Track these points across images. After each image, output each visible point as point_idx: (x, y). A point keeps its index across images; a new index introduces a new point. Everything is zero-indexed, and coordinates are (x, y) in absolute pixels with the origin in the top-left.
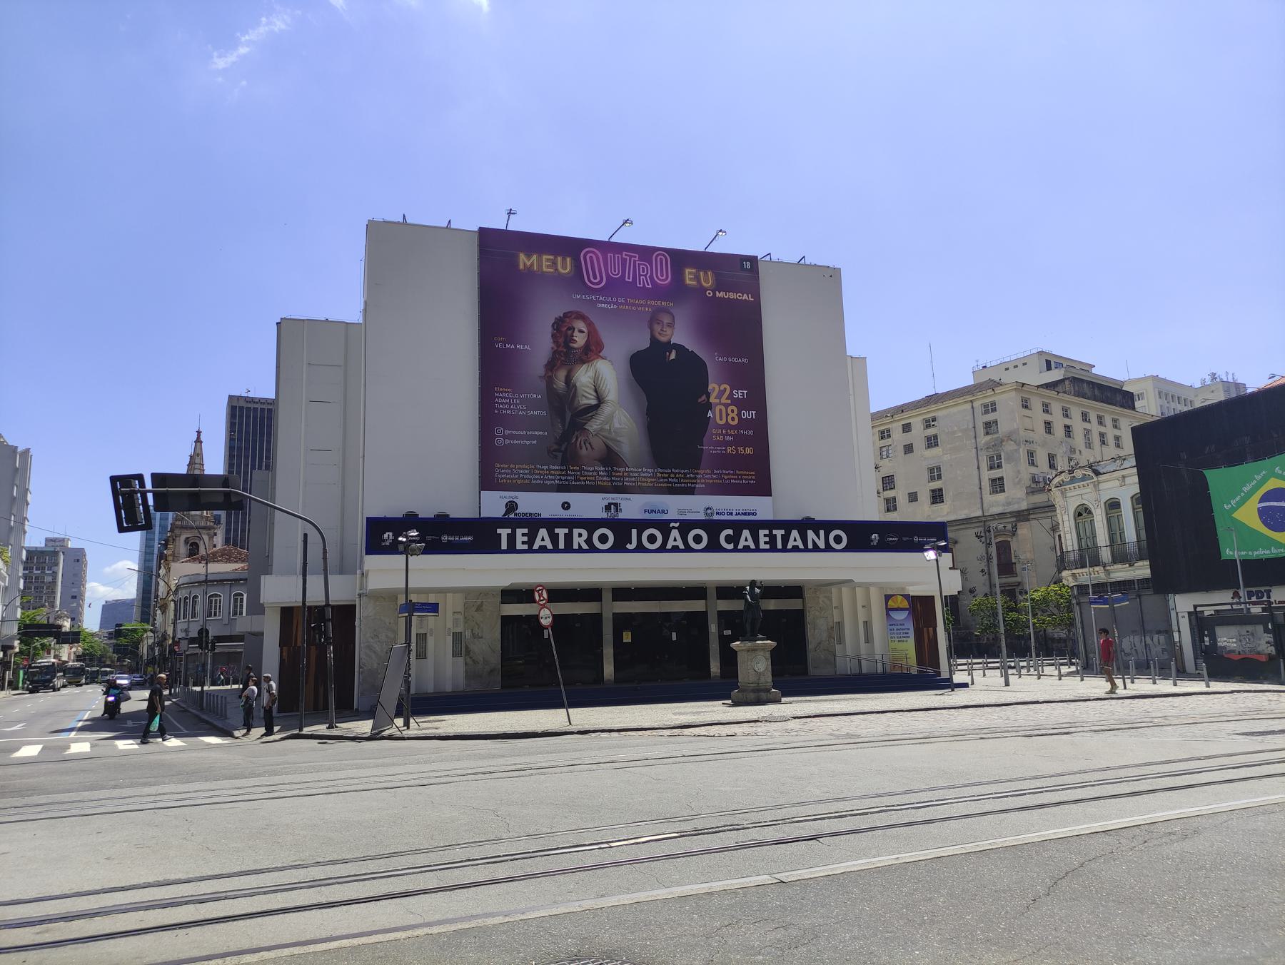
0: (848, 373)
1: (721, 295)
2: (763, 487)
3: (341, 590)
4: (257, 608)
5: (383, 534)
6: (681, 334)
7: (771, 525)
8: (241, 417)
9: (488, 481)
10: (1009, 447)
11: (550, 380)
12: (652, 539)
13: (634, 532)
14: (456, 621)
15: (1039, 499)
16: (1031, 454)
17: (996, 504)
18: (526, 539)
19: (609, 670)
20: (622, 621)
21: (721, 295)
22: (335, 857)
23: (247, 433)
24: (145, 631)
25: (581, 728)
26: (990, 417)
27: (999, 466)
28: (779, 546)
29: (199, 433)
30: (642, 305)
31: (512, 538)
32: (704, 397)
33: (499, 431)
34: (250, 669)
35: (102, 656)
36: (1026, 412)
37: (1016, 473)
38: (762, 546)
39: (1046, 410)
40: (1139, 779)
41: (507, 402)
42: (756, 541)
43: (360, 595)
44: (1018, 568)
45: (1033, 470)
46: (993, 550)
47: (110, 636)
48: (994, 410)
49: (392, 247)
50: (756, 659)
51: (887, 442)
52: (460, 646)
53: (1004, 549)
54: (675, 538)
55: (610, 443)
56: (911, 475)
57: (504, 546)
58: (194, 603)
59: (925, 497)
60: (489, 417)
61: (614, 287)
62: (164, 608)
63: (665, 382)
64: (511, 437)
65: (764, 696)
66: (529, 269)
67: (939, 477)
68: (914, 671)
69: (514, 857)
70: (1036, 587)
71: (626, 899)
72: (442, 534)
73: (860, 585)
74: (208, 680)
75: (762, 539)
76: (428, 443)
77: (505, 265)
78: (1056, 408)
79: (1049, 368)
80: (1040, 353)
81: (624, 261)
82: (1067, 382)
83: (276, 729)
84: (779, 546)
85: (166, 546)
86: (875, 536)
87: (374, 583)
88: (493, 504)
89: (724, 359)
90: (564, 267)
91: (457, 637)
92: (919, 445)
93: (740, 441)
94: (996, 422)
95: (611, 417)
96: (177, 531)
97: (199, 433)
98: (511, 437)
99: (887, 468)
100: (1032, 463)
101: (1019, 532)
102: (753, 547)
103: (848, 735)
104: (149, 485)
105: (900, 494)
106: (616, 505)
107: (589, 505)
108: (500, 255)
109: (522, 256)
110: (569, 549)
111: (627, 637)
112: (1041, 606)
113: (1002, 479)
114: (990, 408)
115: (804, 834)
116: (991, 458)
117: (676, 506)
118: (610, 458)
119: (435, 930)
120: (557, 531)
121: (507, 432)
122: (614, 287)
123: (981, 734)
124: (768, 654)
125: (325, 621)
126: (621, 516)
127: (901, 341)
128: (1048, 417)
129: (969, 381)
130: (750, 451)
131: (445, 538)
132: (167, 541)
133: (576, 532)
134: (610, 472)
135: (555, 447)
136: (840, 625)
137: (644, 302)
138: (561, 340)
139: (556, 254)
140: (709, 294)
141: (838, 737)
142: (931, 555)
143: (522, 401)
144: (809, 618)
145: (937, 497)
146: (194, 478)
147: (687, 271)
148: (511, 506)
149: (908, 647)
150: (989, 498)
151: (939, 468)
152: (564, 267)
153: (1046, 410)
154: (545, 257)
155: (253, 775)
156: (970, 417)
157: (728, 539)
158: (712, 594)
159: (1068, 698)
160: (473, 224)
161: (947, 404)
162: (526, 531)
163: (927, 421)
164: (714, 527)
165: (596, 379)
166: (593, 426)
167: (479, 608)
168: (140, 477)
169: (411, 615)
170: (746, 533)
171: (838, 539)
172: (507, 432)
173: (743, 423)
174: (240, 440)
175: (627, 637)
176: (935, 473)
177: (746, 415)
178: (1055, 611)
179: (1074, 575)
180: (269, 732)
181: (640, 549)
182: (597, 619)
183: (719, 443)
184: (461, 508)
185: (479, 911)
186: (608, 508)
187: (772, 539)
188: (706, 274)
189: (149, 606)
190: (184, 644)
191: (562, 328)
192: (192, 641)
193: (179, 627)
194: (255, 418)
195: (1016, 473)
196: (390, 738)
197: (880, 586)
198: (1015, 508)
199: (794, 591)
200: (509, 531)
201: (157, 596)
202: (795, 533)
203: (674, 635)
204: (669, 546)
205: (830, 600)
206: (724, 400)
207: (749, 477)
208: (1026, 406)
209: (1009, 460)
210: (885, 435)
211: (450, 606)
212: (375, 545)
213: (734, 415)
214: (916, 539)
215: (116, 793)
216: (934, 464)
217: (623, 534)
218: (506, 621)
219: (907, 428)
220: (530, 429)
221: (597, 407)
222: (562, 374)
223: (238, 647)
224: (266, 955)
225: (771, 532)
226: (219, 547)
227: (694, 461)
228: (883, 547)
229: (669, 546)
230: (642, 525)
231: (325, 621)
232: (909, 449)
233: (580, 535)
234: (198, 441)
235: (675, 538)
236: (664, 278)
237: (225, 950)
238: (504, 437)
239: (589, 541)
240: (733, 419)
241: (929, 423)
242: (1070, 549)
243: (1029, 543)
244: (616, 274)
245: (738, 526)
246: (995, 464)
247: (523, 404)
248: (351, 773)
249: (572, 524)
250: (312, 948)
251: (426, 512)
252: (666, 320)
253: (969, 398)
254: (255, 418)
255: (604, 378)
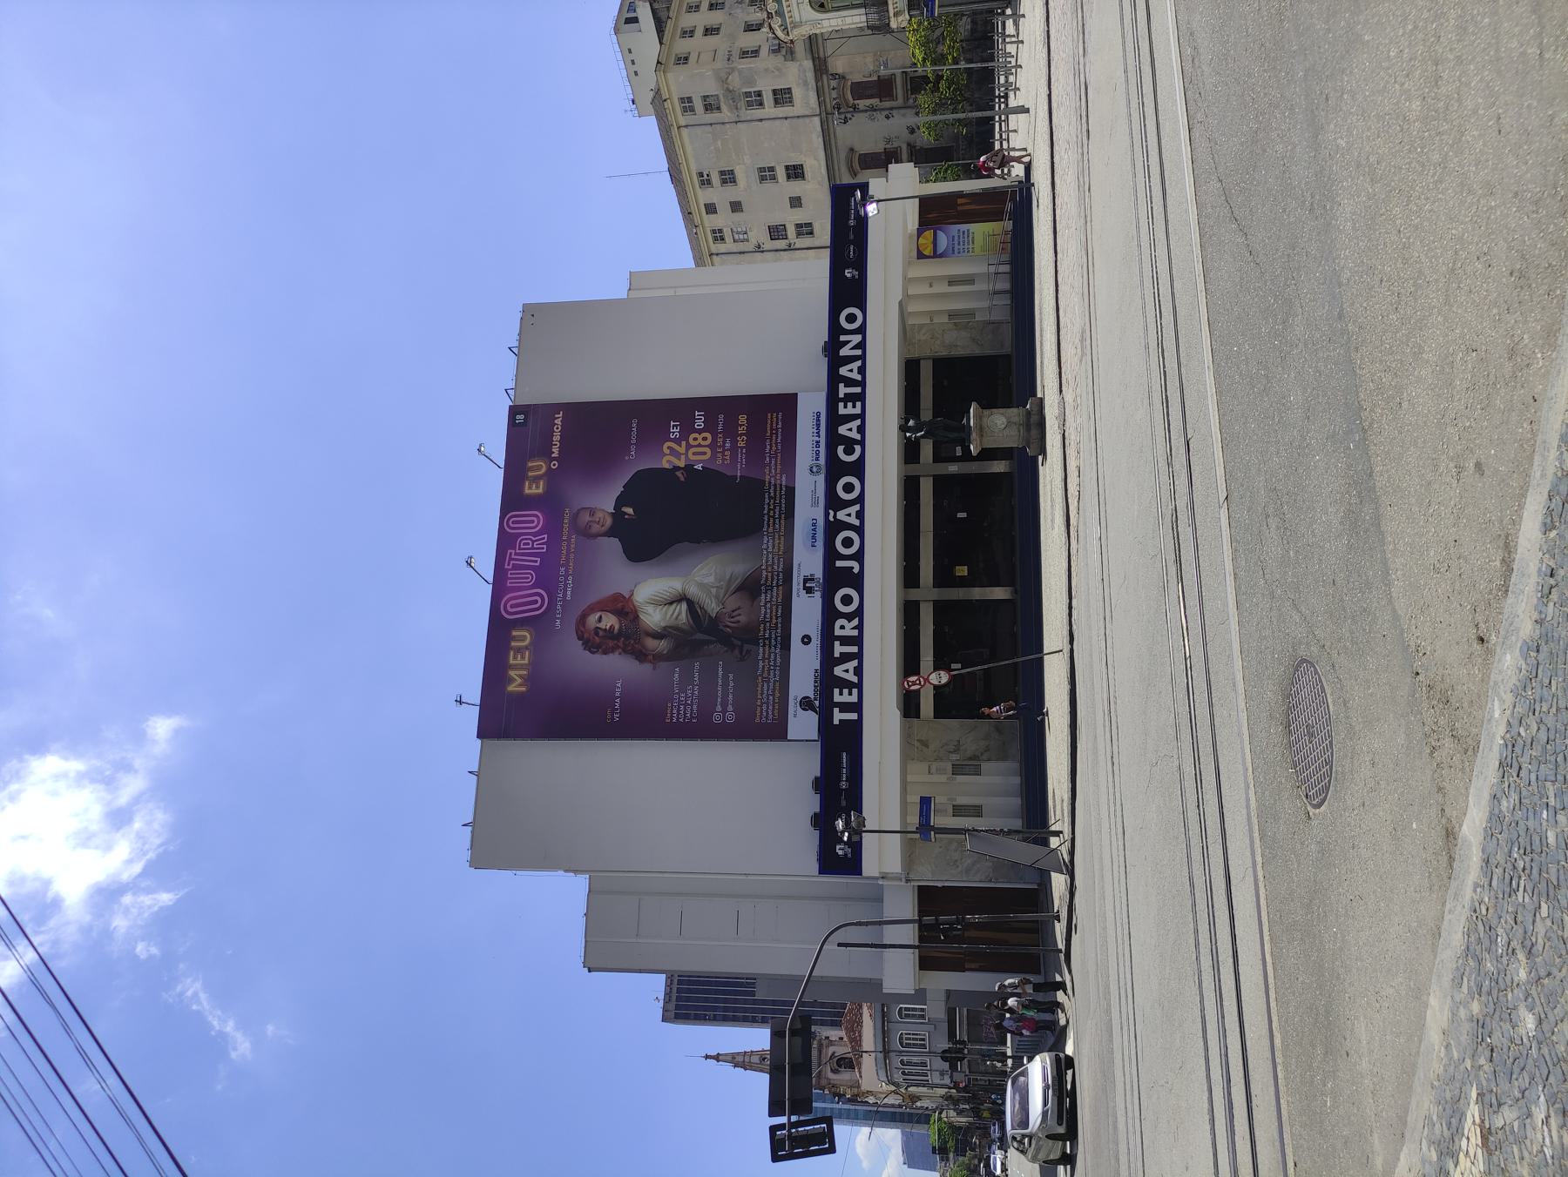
0: (645, 302)
1: (556, 450)
2: (786, 404)
3: (902, 904)
4: (920, 996)
5: (839, 857)
6: (604, 500)
7: (832, 400)
8: (687, 1007)
9: (776, 731)
10: (735, 81)
11: (658, 657)
12: (848, 543)
13: (839, 564)
14: (940, 771)
15: (800, 49)
16: (744, 54)
17: (805, 99)
18: (846, 691)
19: (1000, 593)
20: (943, 577)
21: (556, 450)
22: (1192, 941)
23: (706, 1000)
24: (940, 1119)
25: (1067, 640)
26: (698, 105)
27: (759, 94)
28: (858, 390)
29: (707, 1057)
30: (569, 546)
31: (845, 707)
32: (679, 474)
33: (717, 718)
34: (990, 1005)
35: (968, 1169)
36: (693, 59)
37: (768, 74)
38: (858, 410)
39: (689, 33)
40: (1137, 48)
41: (684, 706)
42: (852, 418)
43: (908, 881)
44: (883, 72)
45: (764, 52)
46: (862, 103)
47: (945, 1159)
48: (690, 100)
49: (499, 841)
50: (994, 426)
51: (727, 234)
52: (966, 766)
53: (860, 90)
54: (847, 515)
55: (733, 587)
56: (768, 205)
57: (854, 716)
58: (909, 1064)
59: (796, 188)
60: (700, 729)
61: (547, 578)
62: (915, 1098)
63: (664, 518)
64: (724, 705)
65: (1034, 419)
66: (527, 680)
67: (772, 169)
68: (1009, 225)
69: (1197, 760)
70: (906, 54)
71: (1238, 664)
72: (838, 791)
73: (905, 290)
74: (1000, 1048)
75: (850, 410)
76: (727, 805)
77: (520, 709)
78: (688, 20)
79: (635, 20)
80: (617, 30)
81: (515, 567)
82: (656, 6)
83: (1058, 978)
84: (858, 390)
85: (841, 1096)
86: (848, 273)
87: (894, 865)
88: (803, 724)
89: (633, 448)
90: (523, 639)
91: (958, 770)
92: (731, 193)
93: (731, 432)
94: (705, 98)
95: (701, 586)
96: (824, 1082)
97: (707, 1057)
98: (724, 705)
99: (759, 235)
100: (755, 53)
101: (840, 71)
102: (858, 422)
103: (1082, 340)
104: (783, 1120)
105: (791, 218)
106: (805, 581)
107: (806, 613)
108: (504, 716)
109: (511, 688)
110: (858, 641)
111: (962, 571)
112: (930, 47)
113: (775, 92)
114: (687, 104)
115: (1183, 450)
116: (749, 104)
117: (808, 509)
118: (750, 587)
119: (1259, 859)
120: (837, 655)
121: (719, 708)
122: (547, 578)
123: (1084, 188)
124: (987, 412)
125: (938, 923)
126: (819, 574)
127: (607, 223)
128: (699, 32)
129: (652, 121)
130: (743, 419)
131: (844, 785)
132: (835, 1094)
133: (838, 632)
134: (766, 588)
135: (737, 652)
136: (952, 315)
137: (565, 544)
138: (611, 643)
139: (508, 648)
140: (555, 465)
141: (1083, 354)
142: (872, 209)
143: (683, 690)
144: (944, 353)
145: (795, 172)
146: (774, 1065)
147: (527, 491)
148: (806, 704)
149: (980, 231)
150: (798, 108)
151: (761, 170)
152: (523, 639)
153: (689, 33)
154: (512, 662)
155: (1108, 1011)
156: (698, 130)
157: (849, 451)
158: (913, 469)
159: (1045, 55)
160: (470, 748)
161: (682, 159)
162: (836, 691)
163: (702, 183)
164: (835, 469)
165: (656, 603)
166: (713, 607)
167: (925, 744)
168: (773, 1129)
169: (933, 828)
170: (842, 430)
171: (851, 318)
172: (719, 708)
173: (710, 426)
174: (715, 1009)
175: (962, 571)
176: (766, 174)
177: (700, 423)
178: (938, 32)
179: (896, 15)
180: (1061, 986)
181: (859, 556)
182: (940, 608)
183: (734, 457)
184: (811, 764)
185: (1244, 812)
186: (809, 590)
187: (849, 398)
188: (532, 469)
189: (911, 1115)
190: (958, 1077)
191: (596, 642)
192: (953, 1068)
193: (937, 1081)
194: (690, 991)
195: (768, 74)
196: (1072, 853)
197: (908, 264)
198: (810, 75)
199: (911, 369)
200: (836, 710)
201: (900, 1106)
202: (843, 371)
203: (960, 515)
204: (857, 522)
205: (921, 326)
206: (682, 450)
207: (775, 420)
208: (683, 60)
209: (751, 82)
210: (718, 236)
211: (919, 773)
212: (851, 865)
213: (699, 437)
214: (852, 223)
215: (1123, 1159)
216: (755, 176)
217: (841, 577)
218: (939, 713)
219: (711, 209)
220: (714, 682)
221: (690, 603)
222: (651, 643)
223: (961, 1015)
224: (1275, 1025)
225: (841, 400)
226: (842, 1033)
227: (753, 489)
228: (861, 263)
229: (857, 522)
230: (831, 555)
231: (938, 923)
232: (736, 207)
233: (842, 627)
234: (717, 1058)
235: (847, 515)
236: (536, 519)
237: (1270, 1063)
238: (724, 711)
239: (850, 617)
240: (705, 439)
241: (705, 182)
242: (864, 18)
243: (856, 63)
244: (531, 577)
245: (834, 439)
246: (756, 100)
247: (683, 688)
248: (1109, 907)
249: (828, 637)
250: (1271, 980)
251: (813, 803)
252: (586, 517)
253: (675, 130)
254: (690, 991)
255: (656, 593)
